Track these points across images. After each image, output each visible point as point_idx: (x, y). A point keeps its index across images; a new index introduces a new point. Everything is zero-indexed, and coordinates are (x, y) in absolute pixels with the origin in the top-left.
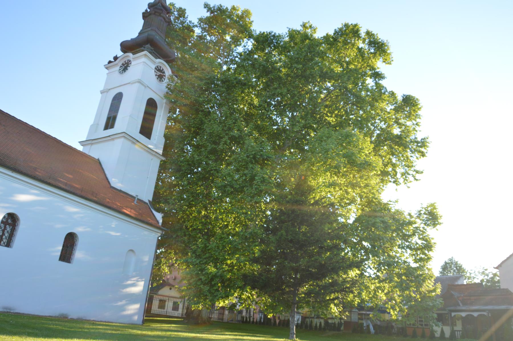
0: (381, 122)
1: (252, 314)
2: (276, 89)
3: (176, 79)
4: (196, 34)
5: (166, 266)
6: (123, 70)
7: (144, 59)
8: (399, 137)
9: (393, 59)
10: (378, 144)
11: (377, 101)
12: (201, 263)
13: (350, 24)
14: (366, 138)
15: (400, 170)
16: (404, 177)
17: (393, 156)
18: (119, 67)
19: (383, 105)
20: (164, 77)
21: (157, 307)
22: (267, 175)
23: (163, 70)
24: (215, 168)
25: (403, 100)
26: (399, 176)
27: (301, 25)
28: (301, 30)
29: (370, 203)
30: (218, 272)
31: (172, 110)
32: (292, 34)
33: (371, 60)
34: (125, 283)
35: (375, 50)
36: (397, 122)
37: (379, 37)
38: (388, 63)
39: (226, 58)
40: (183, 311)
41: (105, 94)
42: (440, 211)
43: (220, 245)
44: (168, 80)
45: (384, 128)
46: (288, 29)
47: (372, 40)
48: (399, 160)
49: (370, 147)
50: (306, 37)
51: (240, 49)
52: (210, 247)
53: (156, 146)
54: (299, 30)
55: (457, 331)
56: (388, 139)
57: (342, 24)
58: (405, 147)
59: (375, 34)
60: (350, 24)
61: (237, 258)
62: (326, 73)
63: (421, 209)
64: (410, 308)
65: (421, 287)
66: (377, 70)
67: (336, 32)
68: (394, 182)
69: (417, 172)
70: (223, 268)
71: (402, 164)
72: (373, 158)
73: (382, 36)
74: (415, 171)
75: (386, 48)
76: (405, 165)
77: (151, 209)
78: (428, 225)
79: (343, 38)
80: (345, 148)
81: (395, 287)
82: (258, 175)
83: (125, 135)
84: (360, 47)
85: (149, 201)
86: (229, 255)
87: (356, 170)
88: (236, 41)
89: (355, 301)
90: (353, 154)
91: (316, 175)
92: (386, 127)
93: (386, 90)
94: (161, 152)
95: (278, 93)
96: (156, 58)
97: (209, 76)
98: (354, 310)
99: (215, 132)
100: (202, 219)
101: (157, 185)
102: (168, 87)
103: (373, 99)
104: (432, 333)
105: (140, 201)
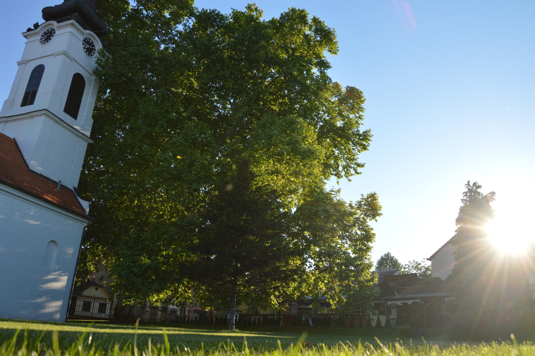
0: (325, 113)
1: (187, 314)
2: (218, 71)
3: (107, 54)
4: (130, 7)
5: (92, 263)
6: (45, 40)
7: (70, 29)
8: (342, 129)
9: (338, 49)
10: (322, 136)
11: (322, 90)
12: (134, 254)
13: (297, 9)
14: (310, 127)
15: (342, 163)
16: (346, 170)
17: (335, 148)
18: (40, 36)
19: (327, 95)
20: (93, 51)
21: (81, 308)
22: (207, 160)
23: (92, 42)
24: (150, 153)
25: (347, 91)
26: (340, 168)
27: (246, 7)
28: (246, 12)
29: (312, 192)
30: (152, 264)
31: (101, 91)
32: (237, 15)
33: (317, 48)
34: (45, 278)
35: (321, 38)
36: (340, 114)
37: (326, 25)
38: (334, 53)
39: (164, 35)
40: (110, 312)
41: (23, 65)
42: (381, 201)
43: (155, 235)
44: (98, 55)
45: (327, 120)
46: (232, 10)
47: (318, 27)
48: (341, 152)
49: (314, 135)
50: (250, 19)
51: (180, 27)
52: (143, 237)
53: (83, 127)
54: (244, 12)
55: (392, 319)
56: (332, 130)
57: (289, 8)
58: (348, 139)
59: (322, 21)
60: (297, 9)
61: (173, 248)
62: (271, 58)
63: (361, 200)
64: (349, 297)
65: (360, 276)
66: (323, 59)
67: (282, 17)
68: (336, 175)
69: (359, 165)
70: (157, 259)
71: (344, 157)
72: (317, 147)
73: (329, 24)
74: (356, 164)
75: (332, 36)
76: (346, 158)
77: (77, 196)
78: (368, 216)
79: (289, 24)
80: (288, 135)
81: (336, 277)
82: (198, 160)
83: (47, 112)
84: (306, 34)
85: (74, 188)
86: (164, 245)
87: (299, 158)
88: (176, 18)
89: (295, 294)
90: (297, 141)
91: (258, 162)
92: (329, 119)
93: (331, 81)
94: (88, 134)
95: (220, 75)
96: (85, 29)
97: (145, 53)
98: (293, 304)
99: (151, 113)
100: (134, 209)
101: (83, 173)
102: (98, 62)
103: (318, 88)
104: (369, 321)
105: (63, 187)
